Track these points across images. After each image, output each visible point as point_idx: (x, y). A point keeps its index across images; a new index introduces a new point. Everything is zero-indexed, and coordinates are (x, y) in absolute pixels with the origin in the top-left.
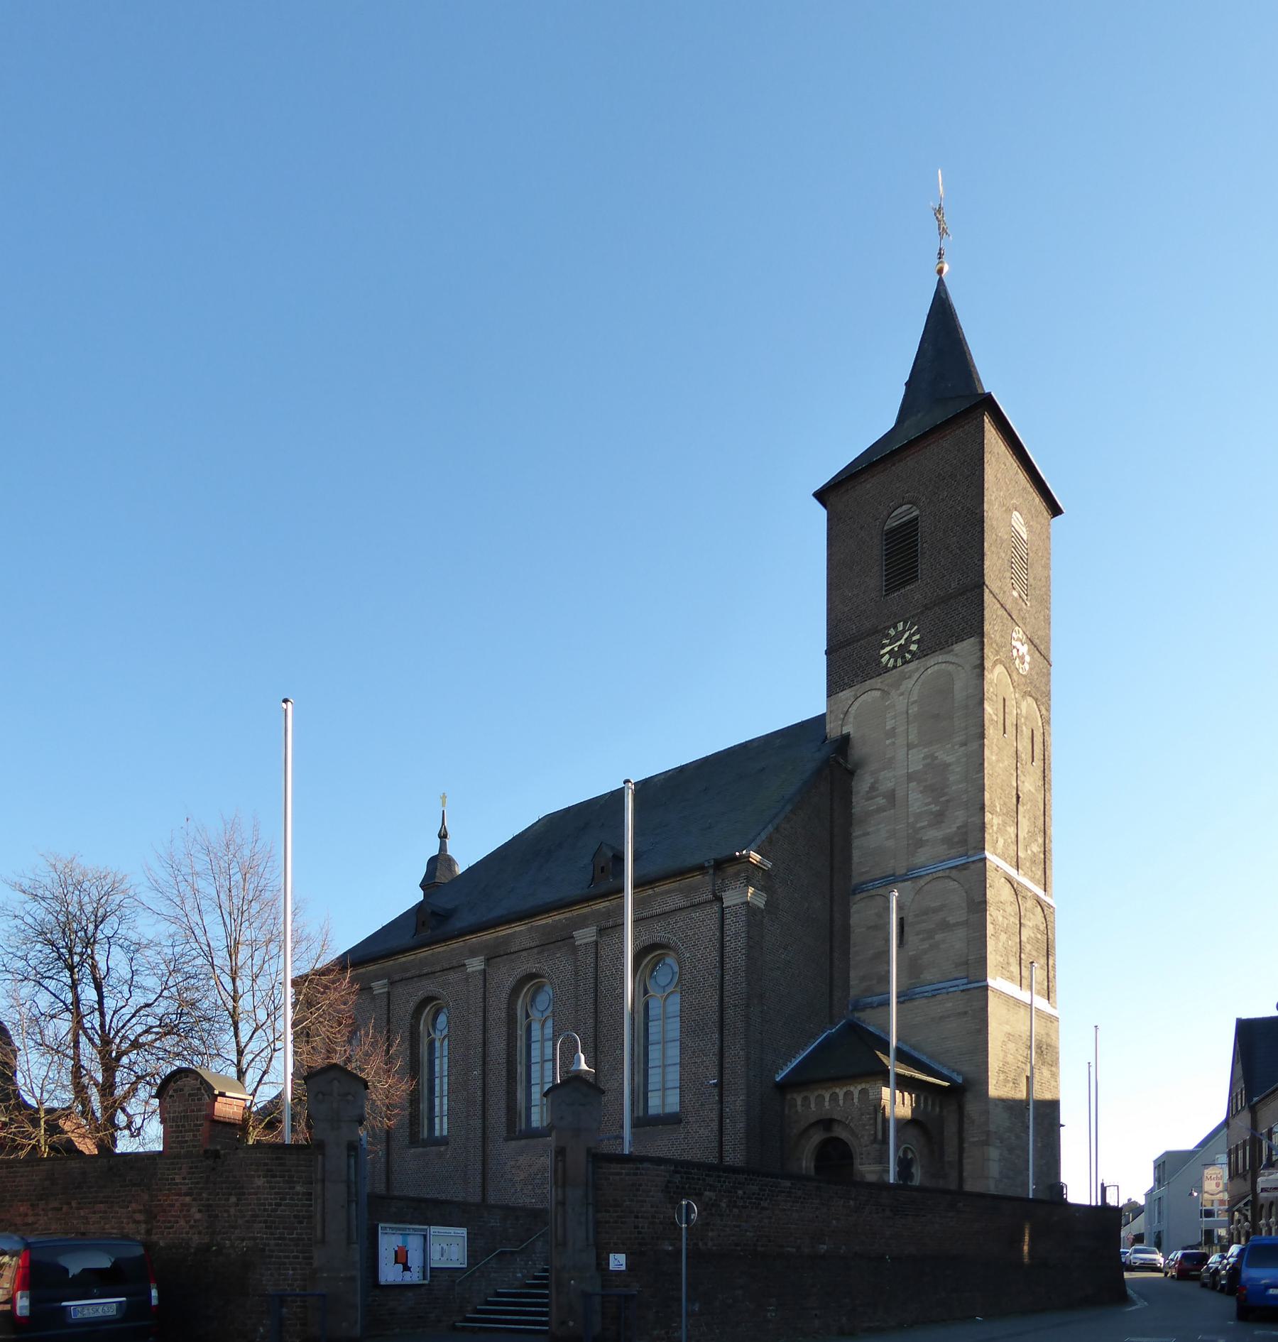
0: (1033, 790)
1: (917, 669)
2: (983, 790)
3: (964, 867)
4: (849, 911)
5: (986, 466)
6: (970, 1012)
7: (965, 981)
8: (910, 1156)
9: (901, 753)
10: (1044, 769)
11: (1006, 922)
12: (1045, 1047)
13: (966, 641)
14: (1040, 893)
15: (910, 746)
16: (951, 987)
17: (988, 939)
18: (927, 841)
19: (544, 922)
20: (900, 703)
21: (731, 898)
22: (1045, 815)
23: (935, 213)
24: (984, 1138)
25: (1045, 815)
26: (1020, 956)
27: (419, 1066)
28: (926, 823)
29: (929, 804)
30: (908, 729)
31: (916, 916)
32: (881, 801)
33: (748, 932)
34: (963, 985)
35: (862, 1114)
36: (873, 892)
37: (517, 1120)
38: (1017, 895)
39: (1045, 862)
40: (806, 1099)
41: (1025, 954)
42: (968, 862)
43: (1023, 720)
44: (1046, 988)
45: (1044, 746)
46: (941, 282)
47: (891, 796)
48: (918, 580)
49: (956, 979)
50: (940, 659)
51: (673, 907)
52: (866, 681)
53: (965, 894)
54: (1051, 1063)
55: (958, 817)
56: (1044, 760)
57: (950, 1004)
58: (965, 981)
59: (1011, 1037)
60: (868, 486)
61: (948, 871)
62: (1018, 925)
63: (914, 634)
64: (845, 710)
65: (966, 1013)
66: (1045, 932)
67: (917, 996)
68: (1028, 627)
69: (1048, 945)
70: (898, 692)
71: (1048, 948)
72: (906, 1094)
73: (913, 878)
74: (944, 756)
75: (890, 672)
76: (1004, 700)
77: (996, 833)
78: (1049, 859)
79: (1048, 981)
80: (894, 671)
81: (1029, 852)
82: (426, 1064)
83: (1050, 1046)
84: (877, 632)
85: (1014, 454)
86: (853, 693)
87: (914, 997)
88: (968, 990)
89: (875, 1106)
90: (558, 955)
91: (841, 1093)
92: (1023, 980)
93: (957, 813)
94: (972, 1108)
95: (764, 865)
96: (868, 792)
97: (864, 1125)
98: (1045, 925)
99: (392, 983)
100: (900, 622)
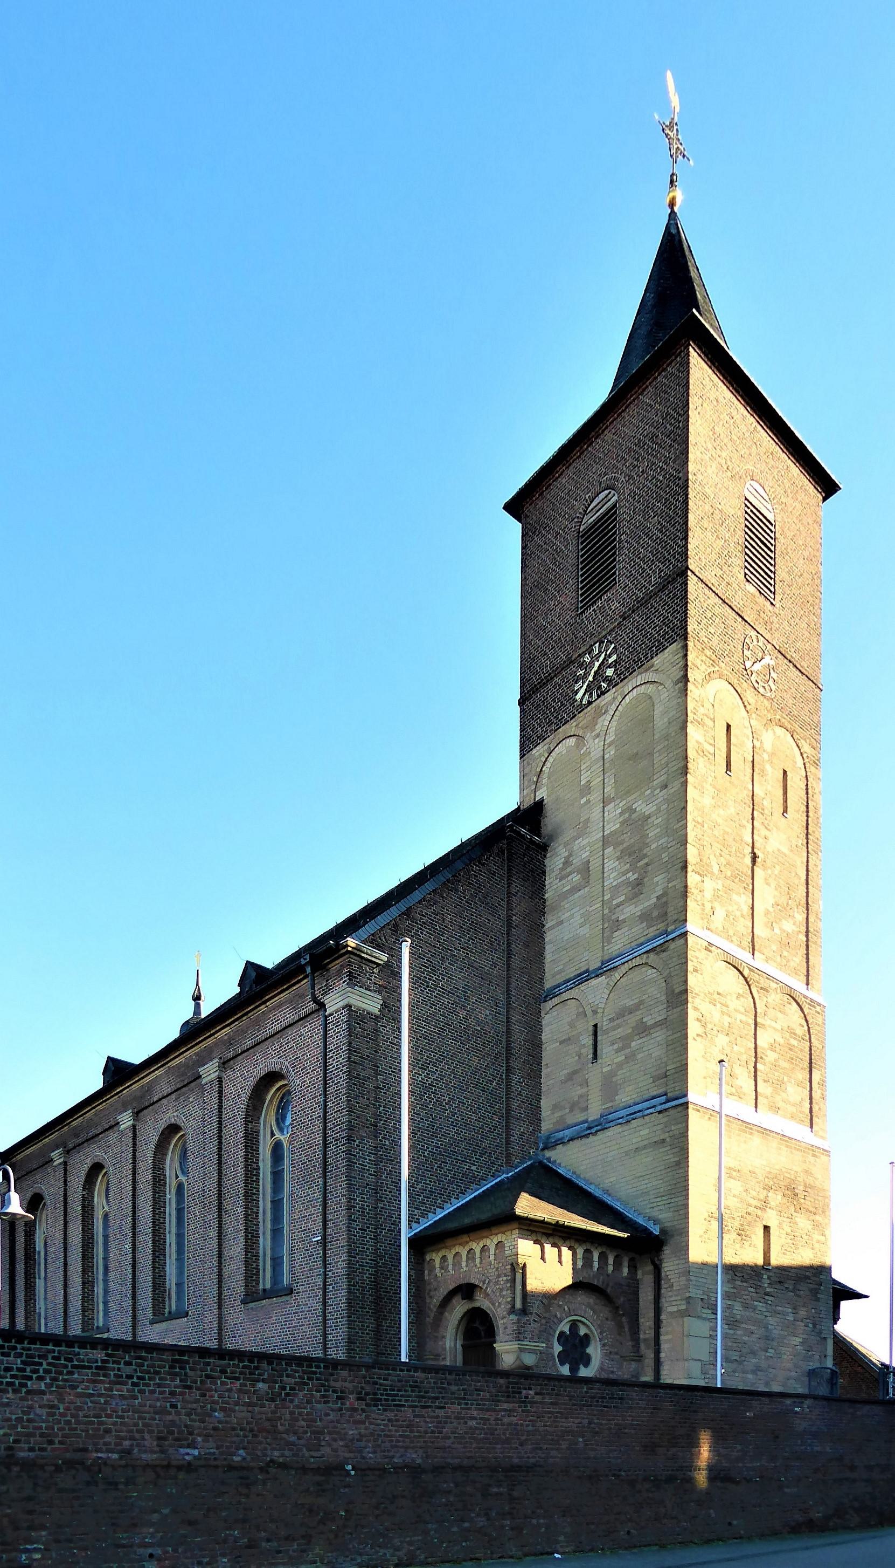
0: (785, 850)
1: (614, 699)
2: (684, 842)
3: (662, 948)
4: (539, 1023)
5: (692, 413)
6: (668, 1139)
7: (663, 1099)
8: (582, 1331)
9: (596, 813)
10: (807, 824)
11: (727, 1020)
12: (801, 1188)
13: (668, 650)
14: (798, 985)
15: (605, 802)
16: (648, 1109)
17: (690, 1040)
18: (624, 921)
19: (177, 1061)
20: (594, 746)
21: (334, 1002)
22: (807, 884)
23: (663, 130)
24: (684, 1307)
25: (807, 884)
26: (755, 1067)
27: (93, 1243)
28: (623, 898)
29: (627, 871)
30: (604, 779)
31: (611, 1020)
32: (576, 878)
33: (350, 1043)
34: (661, 1104)
35: (499, 1276)
36: (565, 996)
37: (167, 1299)
38: (749, 986)
39: (807, 946)
40: (444, 1258)
41: (765, 1064)
42: (667, 941)
43: (766, 756)
44: (807, 1111)
45: (807, 793)
46: (673, 215)
47: (585, 869)
48: (616, 583)
49: (653, 1098)
50: (639, 680)
51: (284, 1024)
52: (560, 727)
53: (664, 984)
54: (813, 1210)
55: (658, 882)
56: (807, 812)
57: (647, 1131)
58: (663, 1099)
59: (734, 1174)
60: (564, 481)
61: (645, 956)
62: (753, 1026)
63: (610, 656)
64: (539, 769)
65: (663, 1141)
66: (807, 1038)
67: (611, 1124)
68: (776, 635)
69: (811, 1054)
70: (593, 734)
71: (811, 1059)
72: (565, 1250)
73: (607, 970)
74: (642, 807)
75: (585, 711)
76: (729, 727)
77: (711, 901)
78: (815, 943)
79: (811, 1103)
80: (589, 708)
81: (777, 931)
82: (101, 1240)
83: (811, 1187)
84: (572, 662)
85: (748, 404)
86: (546, 747)
87: (608, 1125)
88: (666, 1110)
89: (512, 1265)
90: (191, 1100)
91: (476, 1247)
92: (759, 1098)
93: (655, 880)
94: (669, 1266)
95: (375, 957)
96: (562, 869)
97: (501, 1290)
98: (806, 1028)
99: (68, 1152)
100: (596, 643)
